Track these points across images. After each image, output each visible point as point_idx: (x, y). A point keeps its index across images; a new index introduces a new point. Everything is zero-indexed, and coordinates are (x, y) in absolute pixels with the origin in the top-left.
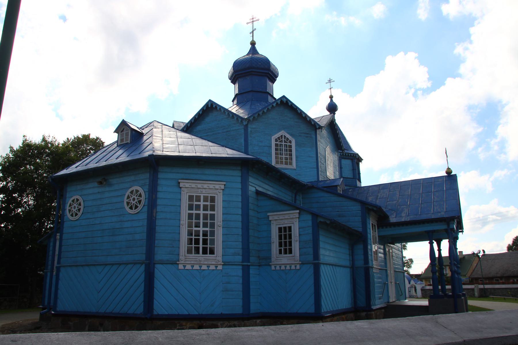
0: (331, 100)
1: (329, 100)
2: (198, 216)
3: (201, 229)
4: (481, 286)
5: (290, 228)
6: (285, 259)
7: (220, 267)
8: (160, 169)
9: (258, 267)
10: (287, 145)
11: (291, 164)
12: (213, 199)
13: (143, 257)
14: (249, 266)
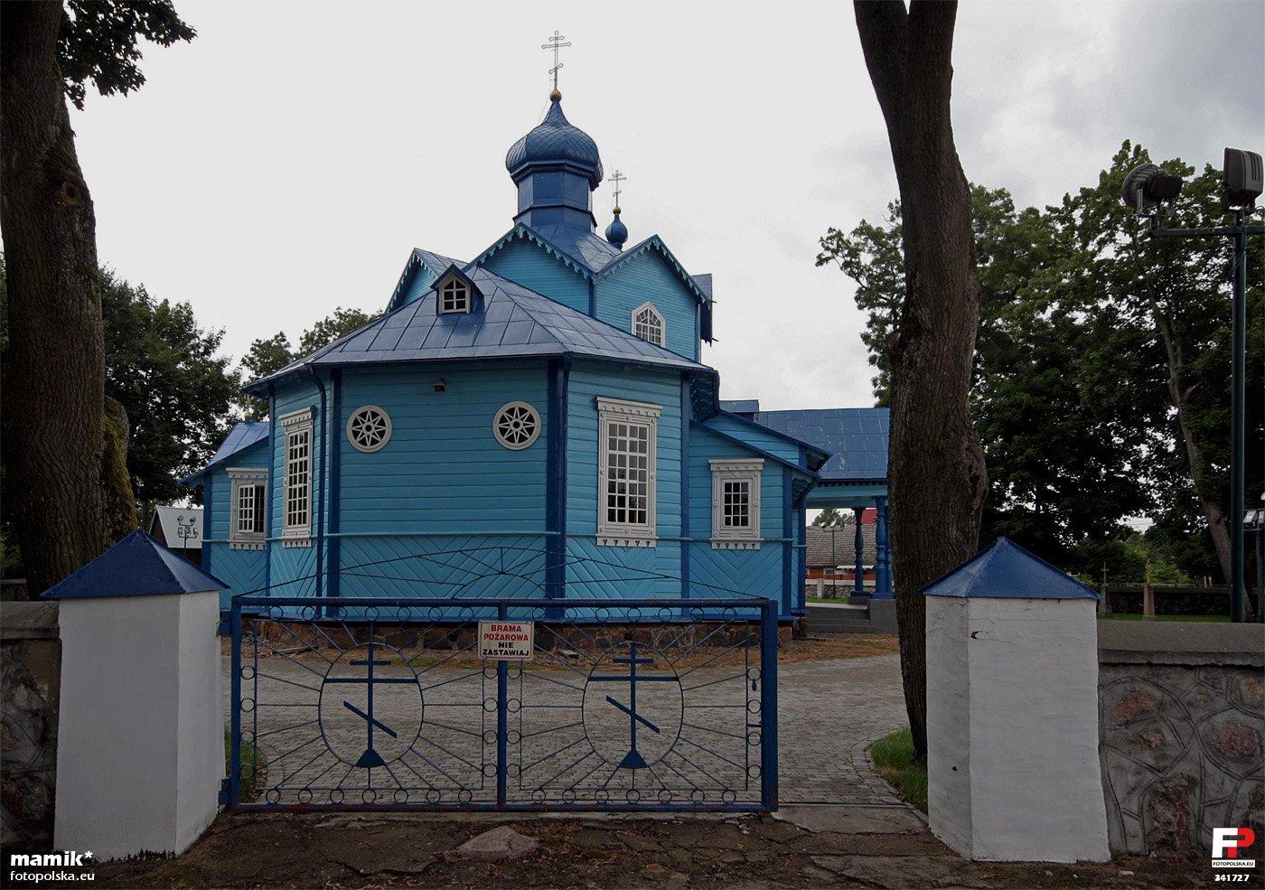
0: (617, 218)
2: (622, 458)
4: (830, 582)
5: (745, 486)
6: (736, 533)
12: (643, 433)
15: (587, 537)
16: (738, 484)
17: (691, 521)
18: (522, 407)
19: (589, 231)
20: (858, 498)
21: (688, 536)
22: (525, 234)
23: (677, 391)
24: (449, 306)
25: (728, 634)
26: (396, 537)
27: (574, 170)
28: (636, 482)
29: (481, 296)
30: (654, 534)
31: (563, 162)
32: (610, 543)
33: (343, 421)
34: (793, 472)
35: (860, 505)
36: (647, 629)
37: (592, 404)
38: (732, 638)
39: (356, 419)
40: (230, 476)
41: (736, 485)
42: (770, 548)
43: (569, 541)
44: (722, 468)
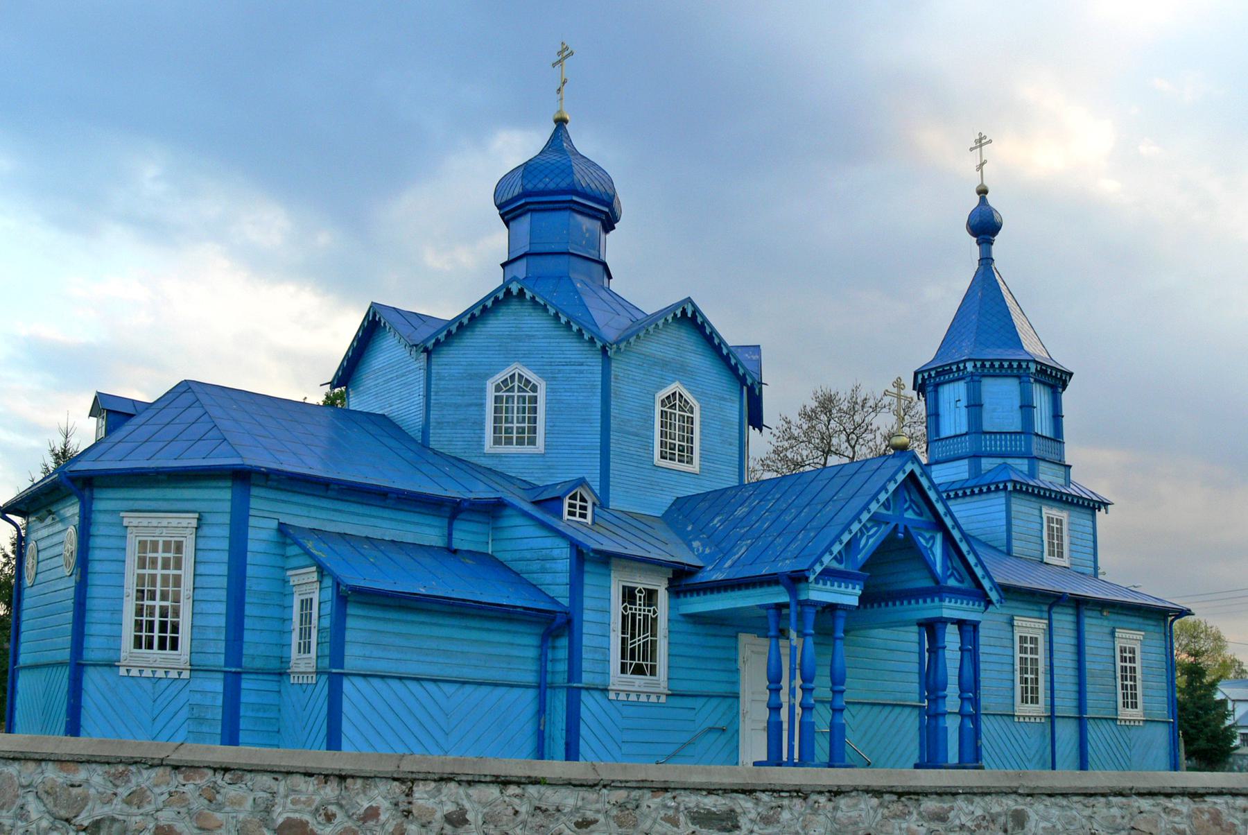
0: (983, 201)
1: (975, 200)
2: (153, 578)
3: (158, 603)
8: (98, 494)
9: (276, 678)
10: (524, 398)
11: (532, 442)
13: (65, 655)
14: (239, 673)
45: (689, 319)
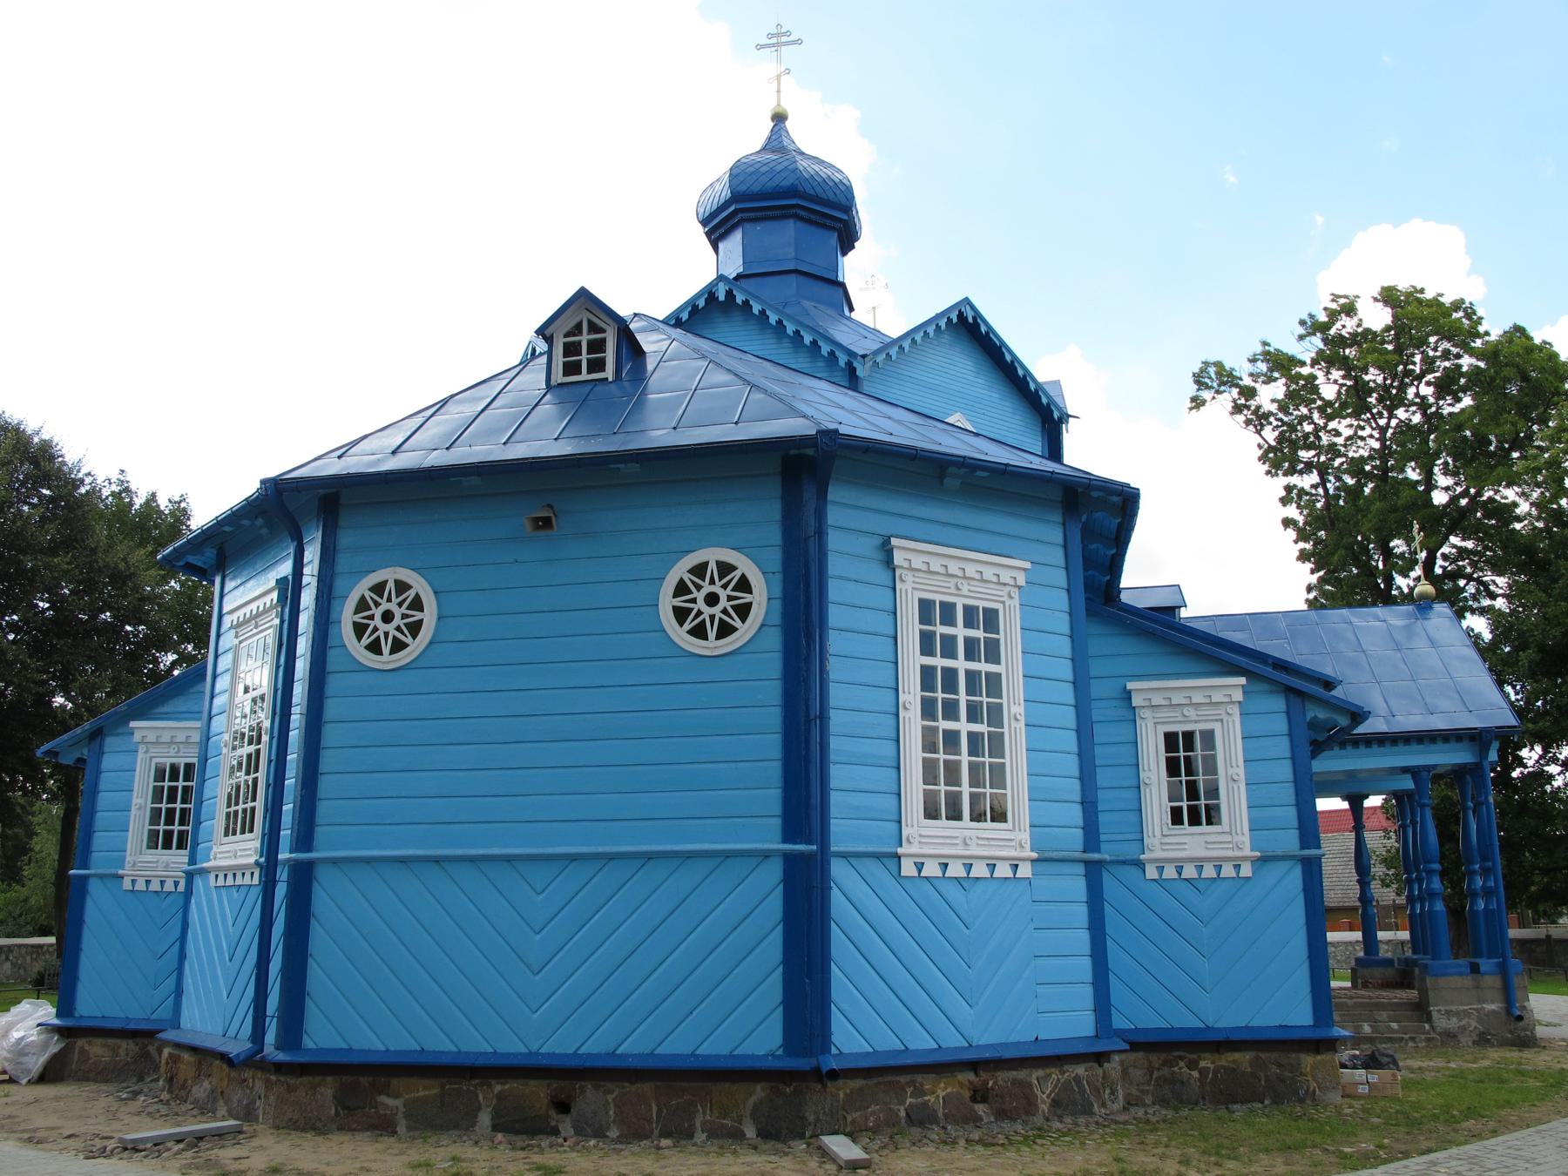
2: (950, 674)
5: (1209, 736)
6: (1194, 842)
7: (1025, 871)
15: (878, 856)
16: (1176, 734)
17: (1102, 818)
18: (723, 559)
19: (842, 314)
20: (1351, 774)
21: (1099, 851)
22: (729, 294)
23: (1056, 535)
24: (571, 369)
25: (1195, 1074)
26: (437, 860)
27: (813, 217)
28: (982, 728)
29: (638, 352)
30: (1028, 846)
31: (793, 202)
32: (932, 869)
33: (335, 604)
34: (1309, 706)
35: (1356, 789)
36: (1021, 1074)
37: (880, 556)
38: (1202, 1084)
39: (363, 597)
40: (137, 737)
41: (1189, 736)
42: (1275, 871)
43: (838, 869)
44: (1158, 700)
45: (967, 329)
